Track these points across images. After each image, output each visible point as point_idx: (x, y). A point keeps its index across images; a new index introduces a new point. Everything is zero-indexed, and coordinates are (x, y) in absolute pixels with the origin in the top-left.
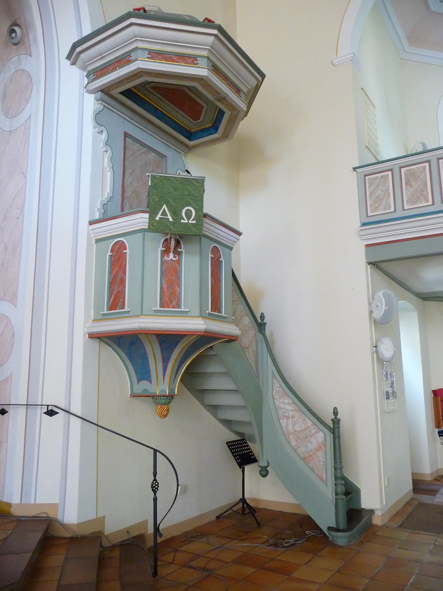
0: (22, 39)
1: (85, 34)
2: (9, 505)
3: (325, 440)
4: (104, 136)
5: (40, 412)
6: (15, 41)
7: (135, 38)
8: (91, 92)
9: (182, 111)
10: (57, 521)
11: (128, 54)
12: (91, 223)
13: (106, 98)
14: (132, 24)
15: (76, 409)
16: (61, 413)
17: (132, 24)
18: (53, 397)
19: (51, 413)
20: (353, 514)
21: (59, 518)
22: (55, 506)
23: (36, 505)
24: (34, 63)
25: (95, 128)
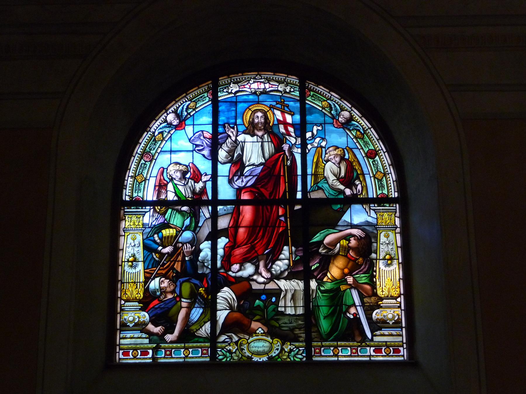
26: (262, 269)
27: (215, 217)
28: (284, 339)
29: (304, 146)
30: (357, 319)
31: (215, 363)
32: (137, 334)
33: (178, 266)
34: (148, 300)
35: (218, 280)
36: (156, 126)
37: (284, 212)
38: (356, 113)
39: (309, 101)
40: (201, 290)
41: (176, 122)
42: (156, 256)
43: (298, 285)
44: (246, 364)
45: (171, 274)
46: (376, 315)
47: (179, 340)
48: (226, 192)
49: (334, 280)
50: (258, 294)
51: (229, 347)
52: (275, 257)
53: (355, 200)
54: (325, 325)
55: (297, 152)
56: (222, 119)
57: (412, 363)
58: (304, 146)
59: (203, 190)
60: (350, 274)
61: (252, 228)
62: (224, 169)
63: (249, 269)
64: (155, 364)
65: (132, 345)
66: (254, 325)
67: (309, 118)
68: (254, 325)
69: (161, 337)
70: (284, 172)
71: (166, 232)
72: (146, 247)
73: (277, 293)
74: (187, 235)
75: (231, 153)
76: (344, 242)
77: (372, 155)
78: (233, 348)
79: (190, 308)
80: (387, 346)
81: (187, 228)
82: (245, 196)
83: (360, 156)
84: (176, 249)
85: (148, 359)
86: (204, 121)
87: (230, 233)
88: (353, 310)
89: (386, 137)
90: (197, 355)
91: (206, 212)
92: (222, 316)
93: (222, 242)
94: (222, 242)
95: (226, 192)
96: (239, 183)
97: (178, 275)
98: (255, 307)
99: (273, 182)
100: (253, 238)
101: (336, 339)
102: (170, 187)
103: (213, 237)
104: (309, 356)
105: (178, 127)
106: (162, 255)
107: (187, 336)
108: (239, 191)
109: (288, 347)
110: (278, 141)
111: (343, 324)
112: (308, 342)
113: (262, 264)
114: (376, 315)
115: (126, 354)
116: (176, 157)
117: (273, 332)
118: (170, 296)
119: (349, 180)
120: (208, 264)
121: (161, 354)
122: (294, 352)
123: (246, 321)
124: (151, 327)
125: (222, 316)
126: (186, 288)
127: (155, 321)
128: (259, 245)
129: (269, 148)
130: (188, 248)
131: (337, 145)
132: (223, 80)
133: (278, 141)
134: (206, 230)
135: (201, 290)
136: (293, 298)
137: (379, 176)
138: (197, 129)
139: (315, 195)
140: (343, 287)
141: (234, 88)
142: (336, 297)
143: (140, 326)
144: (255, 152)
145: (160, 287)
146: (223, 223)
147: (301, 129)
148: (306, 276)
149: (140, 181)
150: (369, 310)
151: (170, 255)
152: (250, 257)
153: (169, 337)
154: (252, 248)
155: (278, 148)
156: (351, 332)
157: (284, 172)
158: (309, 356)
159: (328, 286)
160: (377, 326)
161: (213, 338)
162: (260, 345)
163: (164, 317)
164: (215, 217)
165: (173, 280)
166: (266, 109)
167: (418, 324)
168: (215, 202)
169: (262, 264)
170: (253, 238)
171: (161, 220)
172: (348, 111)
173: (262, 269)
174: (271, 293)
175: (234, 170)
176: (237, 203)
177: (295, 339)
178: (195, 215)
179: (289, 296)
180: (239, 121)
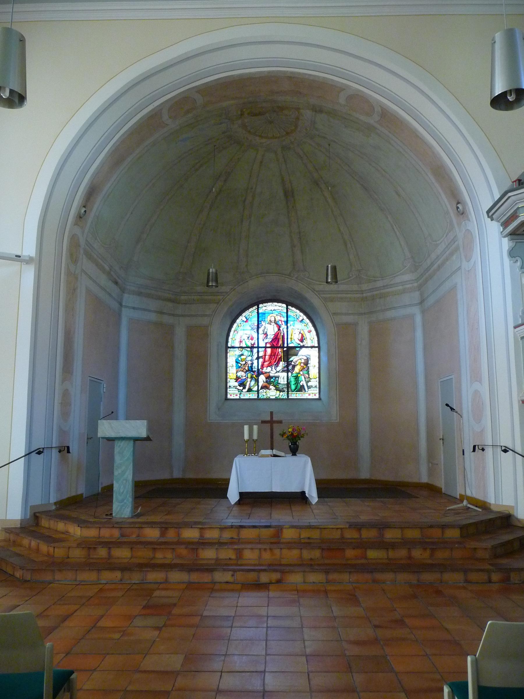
0: (152, 627)
1: (496, 198)
2: (490, 504)
3: (171, 549)
4: (519, 263)
5: (499, 449)
6: (461, 212)
7: (515, 203)
8: (505, 237)
9: (43, 696)
10: (514, 516)
11: (516, 212)
12: (515, 327)
13: (516, 237)
14: (509, 197)
15: (518, 449)
16: (510, 452)
17: (509, 197)
18: (506, 442)
19: (505, 451)
20: (30, 547)
21: (515, 514)
22: (512, 507)
23: (502, 506)
24: (473, 226)
25: (510, 260)
26: (273, 369)
27: (258, 352)
28: (280, 391)
29: (287, 328)
30: (303, 386)
31: (258, 399)
32: (235, 389)
33: (247, 368)
34: (237, 379)
35: (259, 373)
36: (238, 321)
37: (281, 351)
38: (305, 317)
39: (289, 313)
40: (254, 376)
41: (245, 320)
42: (240, 365)
43: (285, 374)
44: (268, 399)
45: (245, 371)
46: (309, 384)
47: (247, 391)
48: (262, 344)
49: (297, 373)
50: (272, 377)
51: (264, 394)
52: (277, 365)
53: (303, 347)
54: (293, 387)
55: (285, 331)
56: (260, 319)
57: (320, 399)
58: (287, 328)
59: (254, 344)
60: (301, 371)
61: (271, 356)
62: (261, 336)
63: (269, 369)
64: (240, 399)
65: (233, 393)
66: (271, 387)
67: (289, 319)
68: (271, 387)
69: (242, 391)
70: (281, 337)
71: (243, 357)
72: (236, 362)
73: (278, 377)
74: (250, 358)
75: (263, 331)
76: (300, 361)
77: (310, 332)
78: (264, 394)
79: (251, 381)
80: (312, 394)
81: (249, 356)
82: (268, 345)
83: (306, 332)
84: (246, 363)
85: (238, 397)
86: (254, 320)
87: (264, 357)
88: (302, 382)
89: (314, 326)
90: (253, 396)
91: (255, 350)
92: (260, 384)
93: (261, 360)
94: (261, 360)
95: (262, 344)
96: (266, 341)
97: (247, 371)
98: (270, 381)
99: (277, 342)
100: (206, 297)
101: (297, 391)
102: (244, 342)
103: (258, 358)
104: (288, 396)
105: (246, 321)
106: (241, 365)
107: (250, 390)
108: (266, 343)
109: (281, 393)
110: (279, 327)
111: (299, 387)
112: (288, 392)
113: (273, 367)
114: (309, 384)
115: (231, 395)
116: (246, 332)
117: (277, 389)
118: (244, 378)
119: (302, 340)
120: (257, 367)
121: (242, 395)
122: (283, 395)
123: (268, 385)
124: (238, 387)
125: (260, 384)
126: (249, 375)
127: (240, 386)
128: (274, 360)
129: (276, 329)
130: (250, 362)
131: (299, 329)
132: (260, 306)
133: (279, 327)
134: (256, 356)
135: (254, 376)
136: (283, 378)
137: (312, 338)
138: (252, 322)
139: (290, 345)
140: (299, 375)
141: (264, 308)
142: (297, 378)
143: (235, 387)
144: (272, 330)
145: (91, 438)
146: (261, 354)
147: (287, 322)
148: (288, 371)
149: (234, 340)
150: (307, 382)
151: (244, 364)
152: (270, 365)
153: (244, 390)
154: (270, 362)
155: (279, 330)
156: (301, 389)
157: (281, 337)
158: (288, 396)
159: (294, 375)
160: (309, 387)
161: (258, 391)
162: (272, 393)
163: (242, 384)
164: (258, 352)
165: (245, 372)
166: (275, 316)
167: (322, 387)
168: (258, 347)
169: (273, 367)
170: (206, 297)
171: (241, 353)
172: (302, 316)
173: (273, 369)
174: (276, 377)
175: (264, 336)
176: (266, 347)
177: (284, 391)
178: (252, 351)
179: (282, 378)
180: (266, 320)
